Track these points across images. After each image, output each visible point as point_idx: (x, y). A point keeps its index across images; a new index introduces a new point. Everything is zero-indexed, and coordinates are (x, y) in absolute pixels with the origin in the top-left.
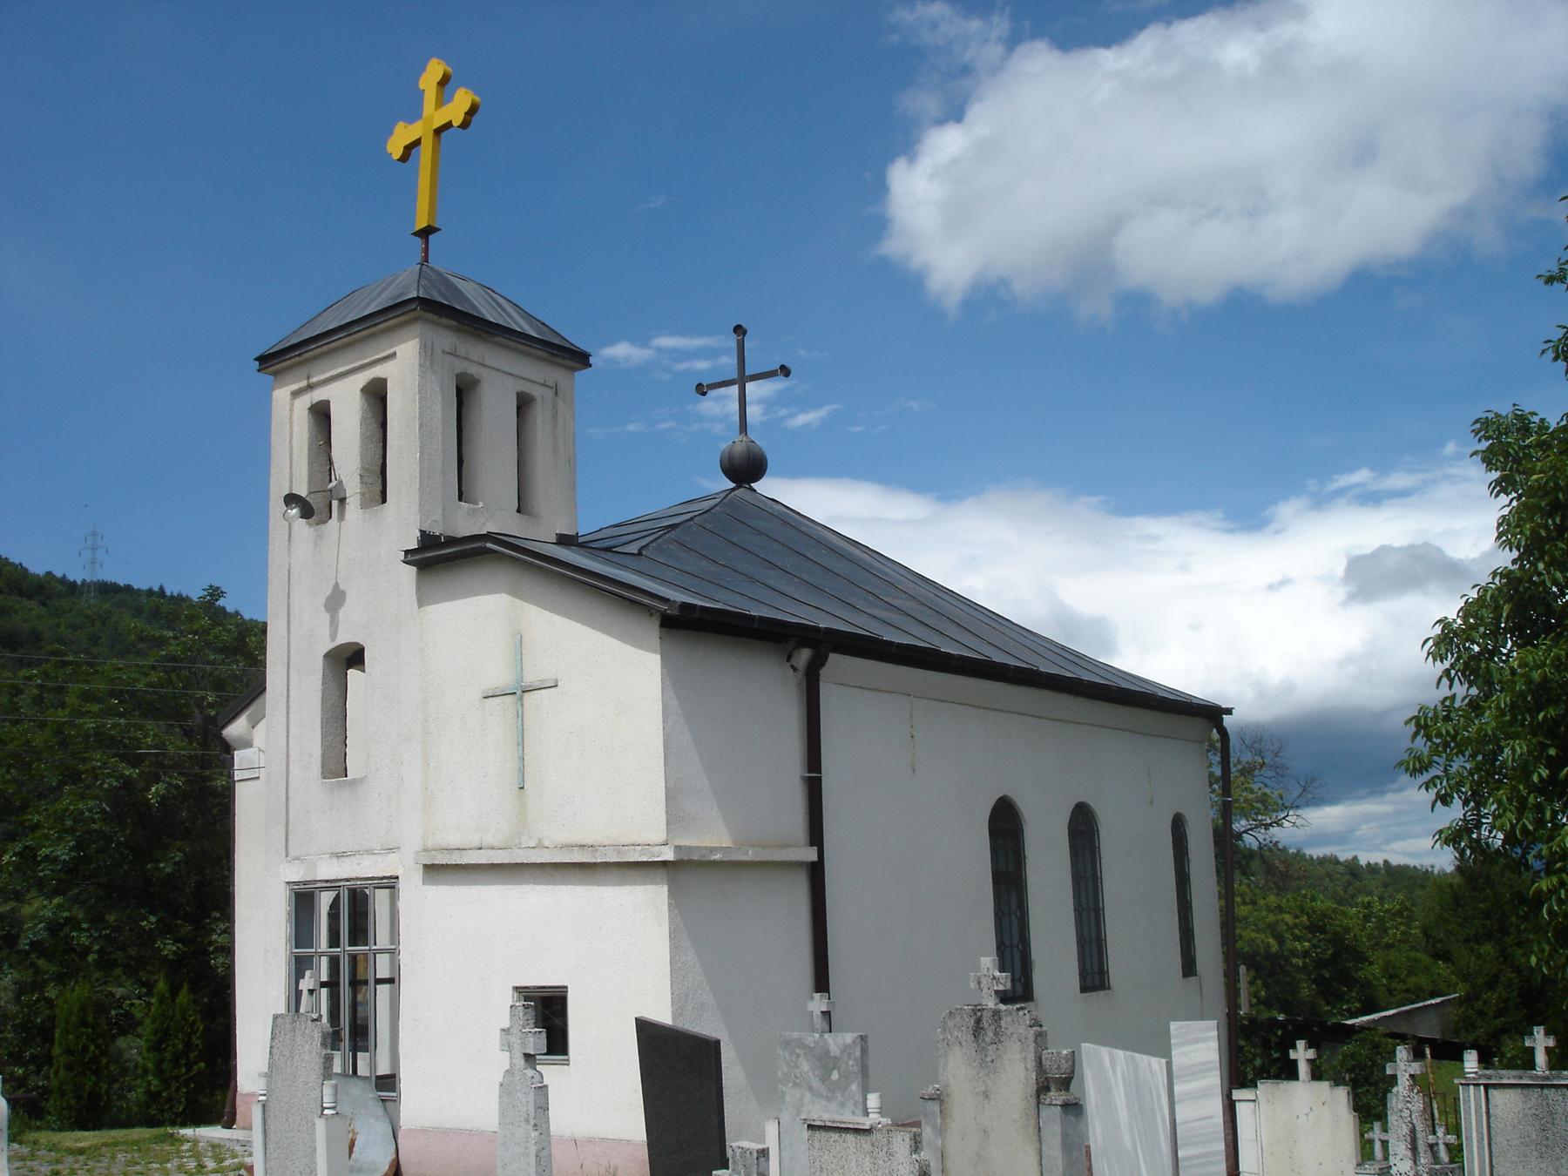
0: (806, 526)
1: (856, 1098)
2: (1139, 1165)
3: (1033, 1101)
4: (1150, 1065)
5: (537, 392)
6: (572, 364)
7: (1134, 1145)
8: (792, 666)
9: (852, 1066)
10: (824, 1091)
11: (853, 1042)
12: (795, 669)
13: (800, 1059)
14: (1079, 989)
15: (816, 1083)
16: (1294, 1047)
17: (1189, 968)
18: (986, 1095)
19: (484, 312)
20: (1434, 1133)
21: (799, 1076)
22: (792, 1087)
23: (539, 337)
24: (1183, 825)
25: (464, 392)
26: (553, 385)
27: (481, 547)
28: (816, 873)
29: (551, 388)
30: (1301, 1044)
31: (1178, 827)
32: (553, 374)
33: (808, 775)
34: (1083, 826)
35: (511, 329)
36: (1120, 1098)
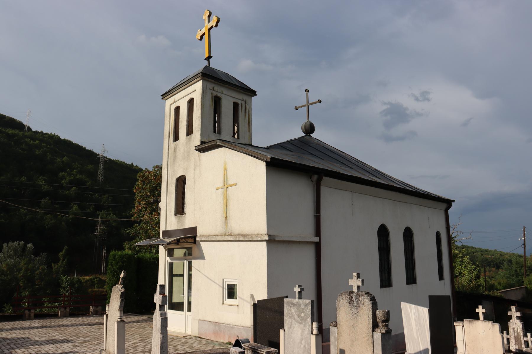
0: (326, 146)
1: (309, 324)
2: (420, 345)
3: (371, 330)
4: (423, 309)
5: (240, 102)
6: (251, 94)
7: (418, 337)
8: (312, 181)
9: (308, 312)
10: (299, 320)
11: (309, 303)
12: (312, 181)
13: (292, 308)
14: (380, 287)
15: (296, 317)
16: (478, 308)
17: (441, 277)
18: (354, 326)
19: (223, 78)
20: (527, 337)
21: (291, 314)
22: (289, 318)
23: (240, 86)
24: (439, 235)
25: (217, 102)
26: (245, 100)
27: (215, 144)
28: (318, 246)
29: (244, 101)
30: (480, 307)
31: (438, 235)
32: (245, 97)
33: (316, 215)
34: (408, 234)
35: (231, 83)
36: (413, 321)
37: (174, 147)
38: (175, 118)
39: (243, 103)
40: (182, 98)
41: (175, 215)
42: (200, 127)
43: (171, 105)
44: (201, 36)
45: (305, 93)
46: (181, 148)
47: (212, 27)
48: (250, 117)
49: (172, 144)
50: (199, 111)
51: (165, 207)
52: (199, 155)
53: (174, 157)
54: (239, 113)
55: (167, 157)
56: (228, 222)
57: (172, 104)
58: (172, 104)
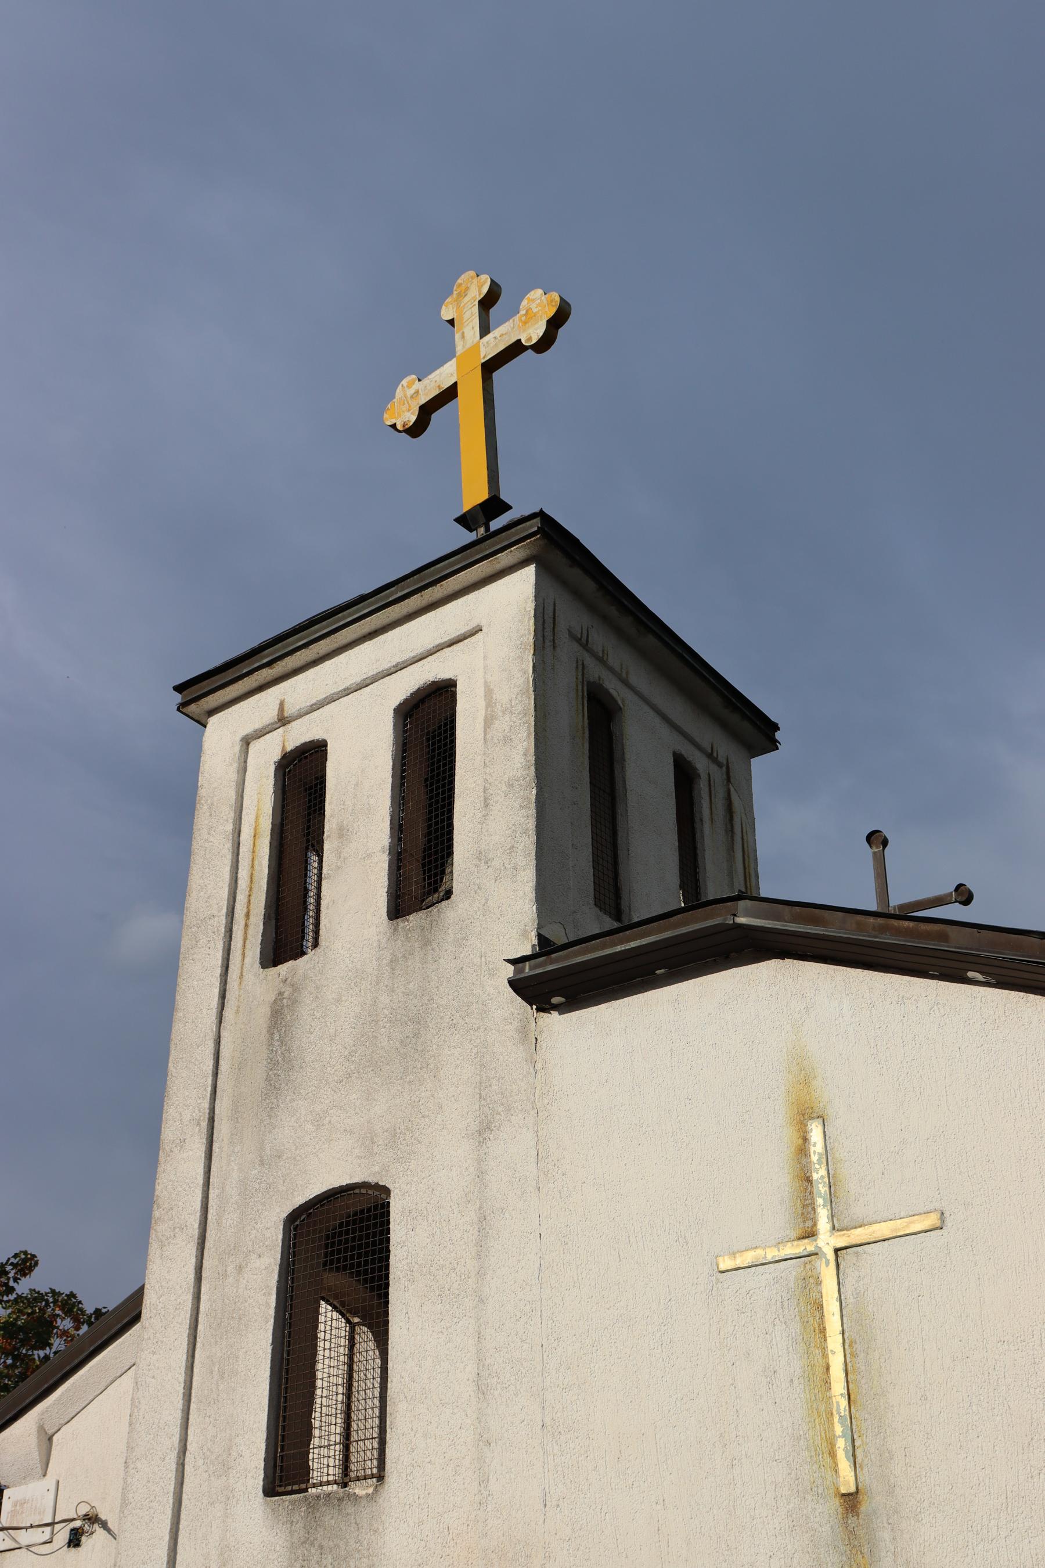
37: (272, 997)
38: (279, 820)
39: (718, 775)
40: (347, 692)
41: (270, 1491)
42: (527, 843)
43: (247, 742)
44: (422, 408)
45: (867, 852)
46: (338, 1001)
47: (516, 349)
48: (752, 865)
49: (249, 977)
50: (520, 749)
51: (176, 1431)
52: (524, 1031)
53: (273, 1063)
54: (697, 825)
55: (210, 1063)
56: (885, 1535)
57: (260, 734)
58: (260, 734)
